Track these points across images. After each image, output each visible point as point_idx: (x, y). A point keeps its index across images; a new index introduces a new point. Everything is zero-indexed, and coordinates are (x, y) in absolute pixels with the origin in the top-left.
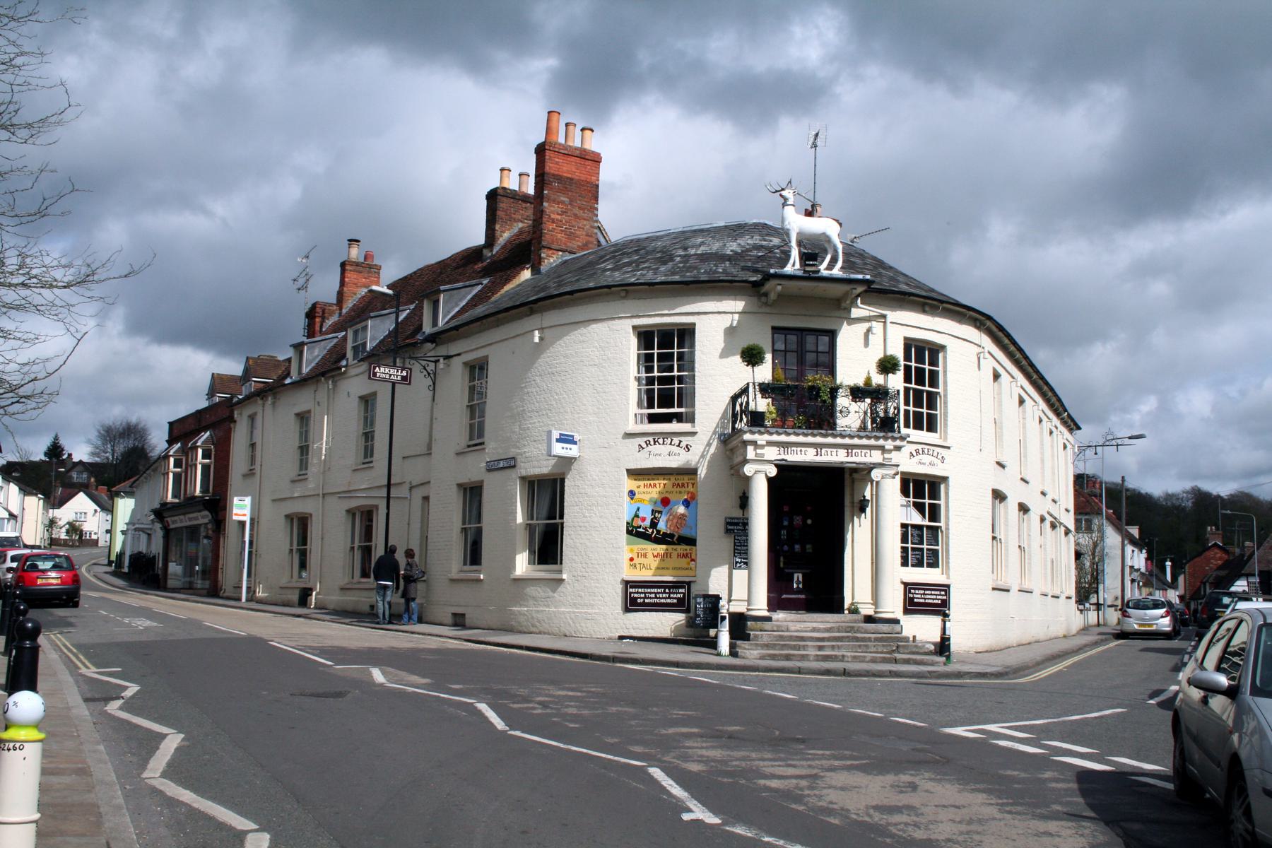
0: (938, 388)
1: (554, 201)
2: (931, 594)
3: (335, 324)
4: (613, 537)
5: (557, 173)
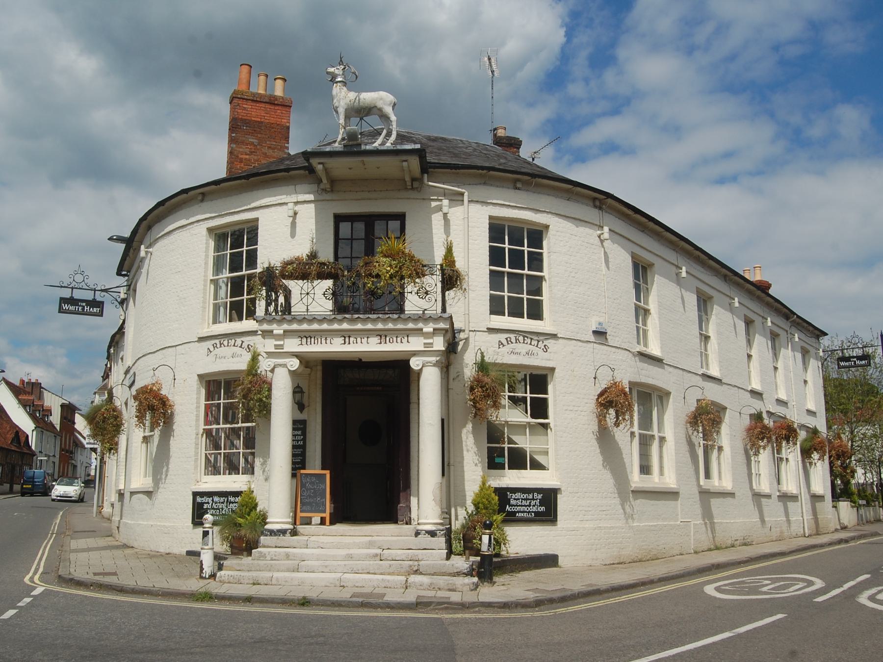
1: (243, 142)
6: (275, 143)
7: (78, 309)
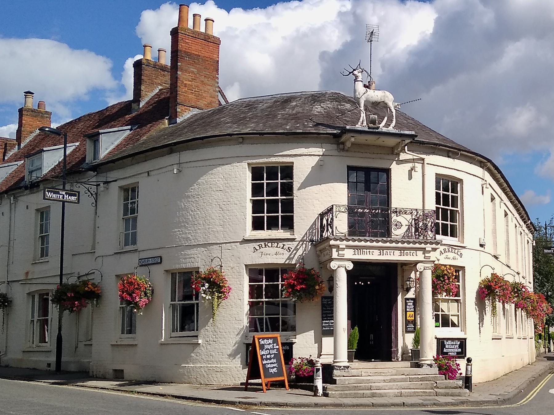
0: (457, 208)
3: (16, 155)
4: (236, 313)
6: (209, 74)
7: (59, 196)
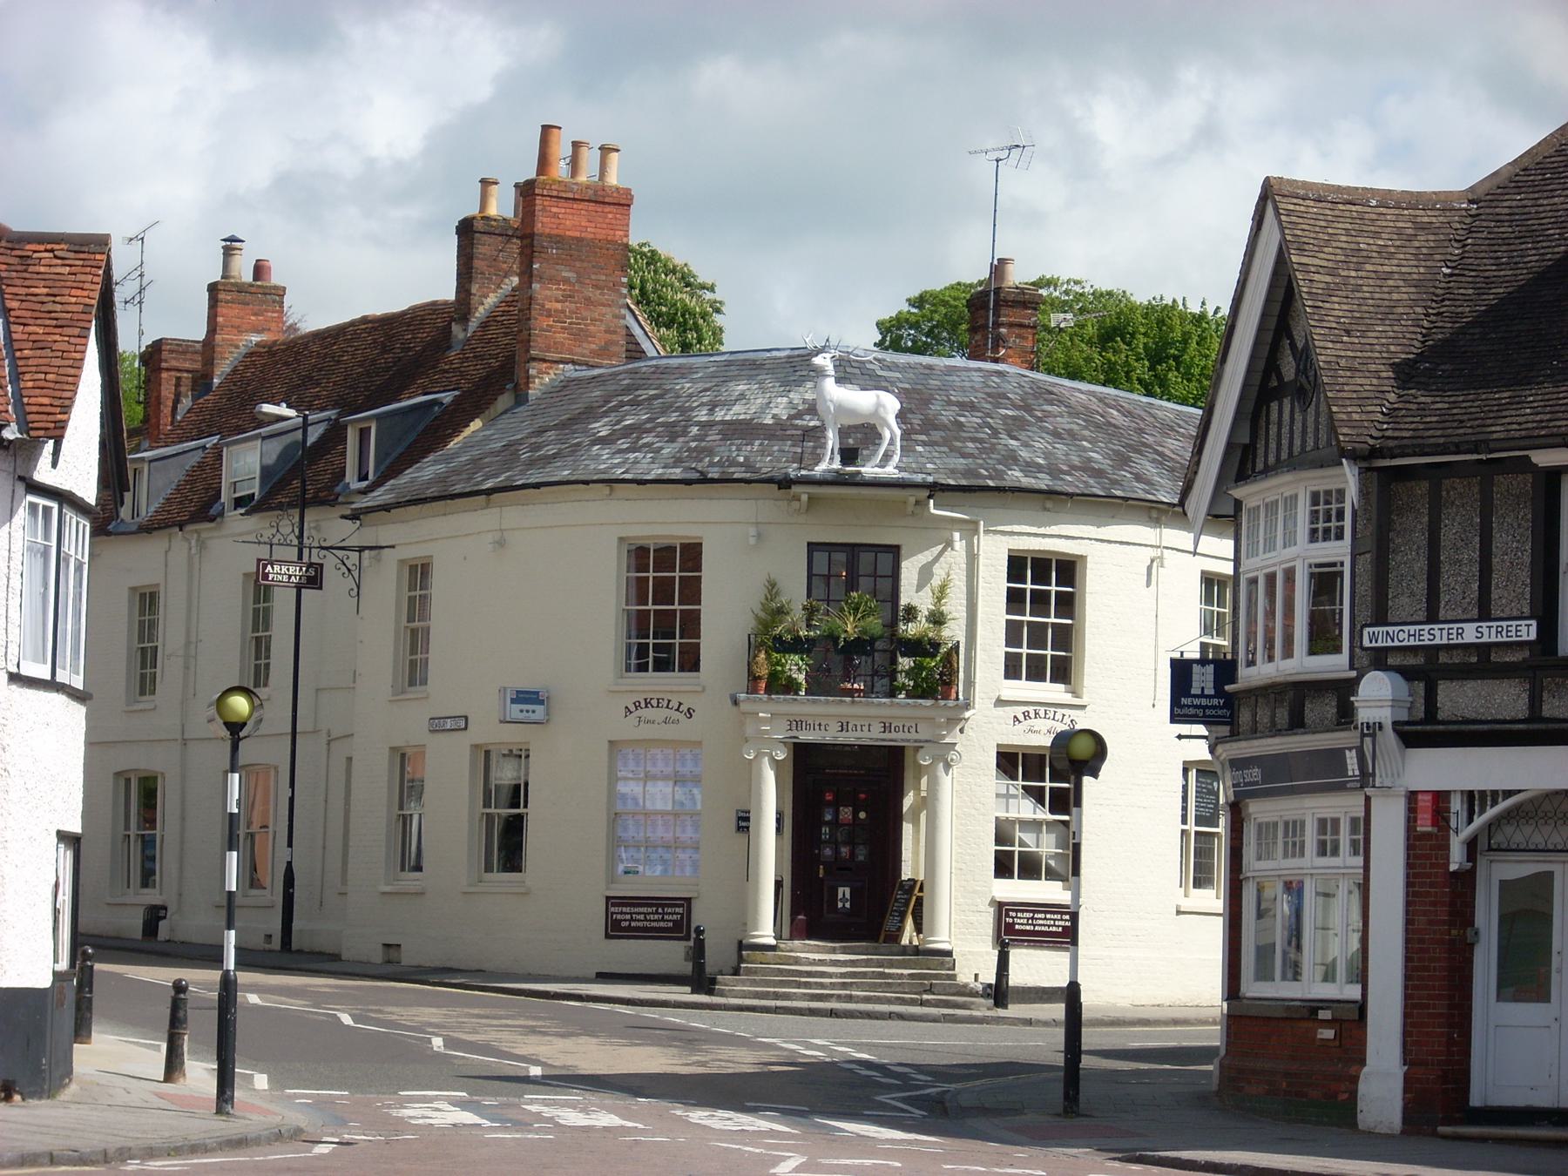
1: (551, 280)
2: (1045, 919)
5: (555, 232)
